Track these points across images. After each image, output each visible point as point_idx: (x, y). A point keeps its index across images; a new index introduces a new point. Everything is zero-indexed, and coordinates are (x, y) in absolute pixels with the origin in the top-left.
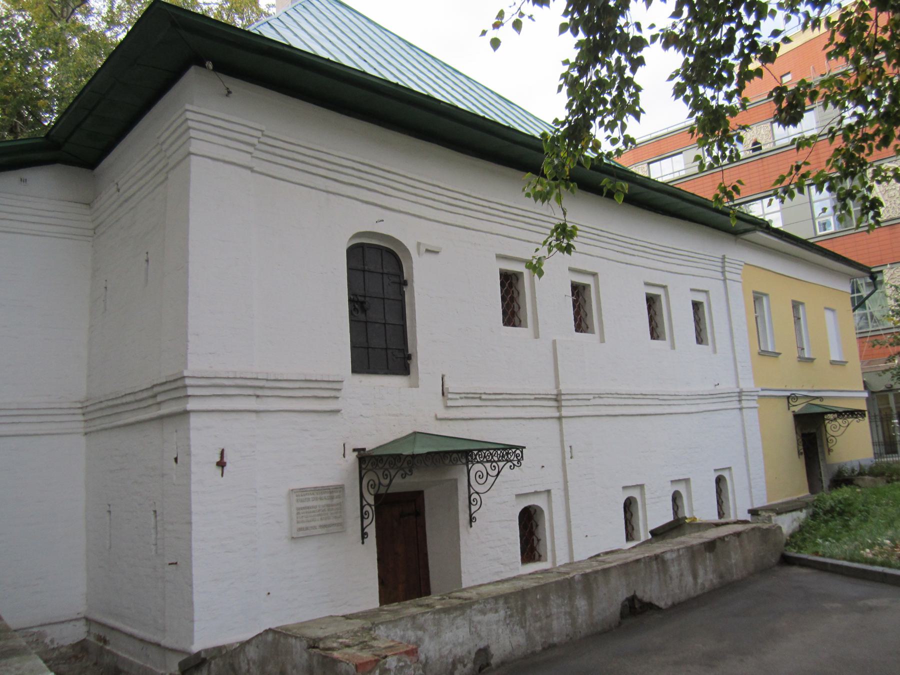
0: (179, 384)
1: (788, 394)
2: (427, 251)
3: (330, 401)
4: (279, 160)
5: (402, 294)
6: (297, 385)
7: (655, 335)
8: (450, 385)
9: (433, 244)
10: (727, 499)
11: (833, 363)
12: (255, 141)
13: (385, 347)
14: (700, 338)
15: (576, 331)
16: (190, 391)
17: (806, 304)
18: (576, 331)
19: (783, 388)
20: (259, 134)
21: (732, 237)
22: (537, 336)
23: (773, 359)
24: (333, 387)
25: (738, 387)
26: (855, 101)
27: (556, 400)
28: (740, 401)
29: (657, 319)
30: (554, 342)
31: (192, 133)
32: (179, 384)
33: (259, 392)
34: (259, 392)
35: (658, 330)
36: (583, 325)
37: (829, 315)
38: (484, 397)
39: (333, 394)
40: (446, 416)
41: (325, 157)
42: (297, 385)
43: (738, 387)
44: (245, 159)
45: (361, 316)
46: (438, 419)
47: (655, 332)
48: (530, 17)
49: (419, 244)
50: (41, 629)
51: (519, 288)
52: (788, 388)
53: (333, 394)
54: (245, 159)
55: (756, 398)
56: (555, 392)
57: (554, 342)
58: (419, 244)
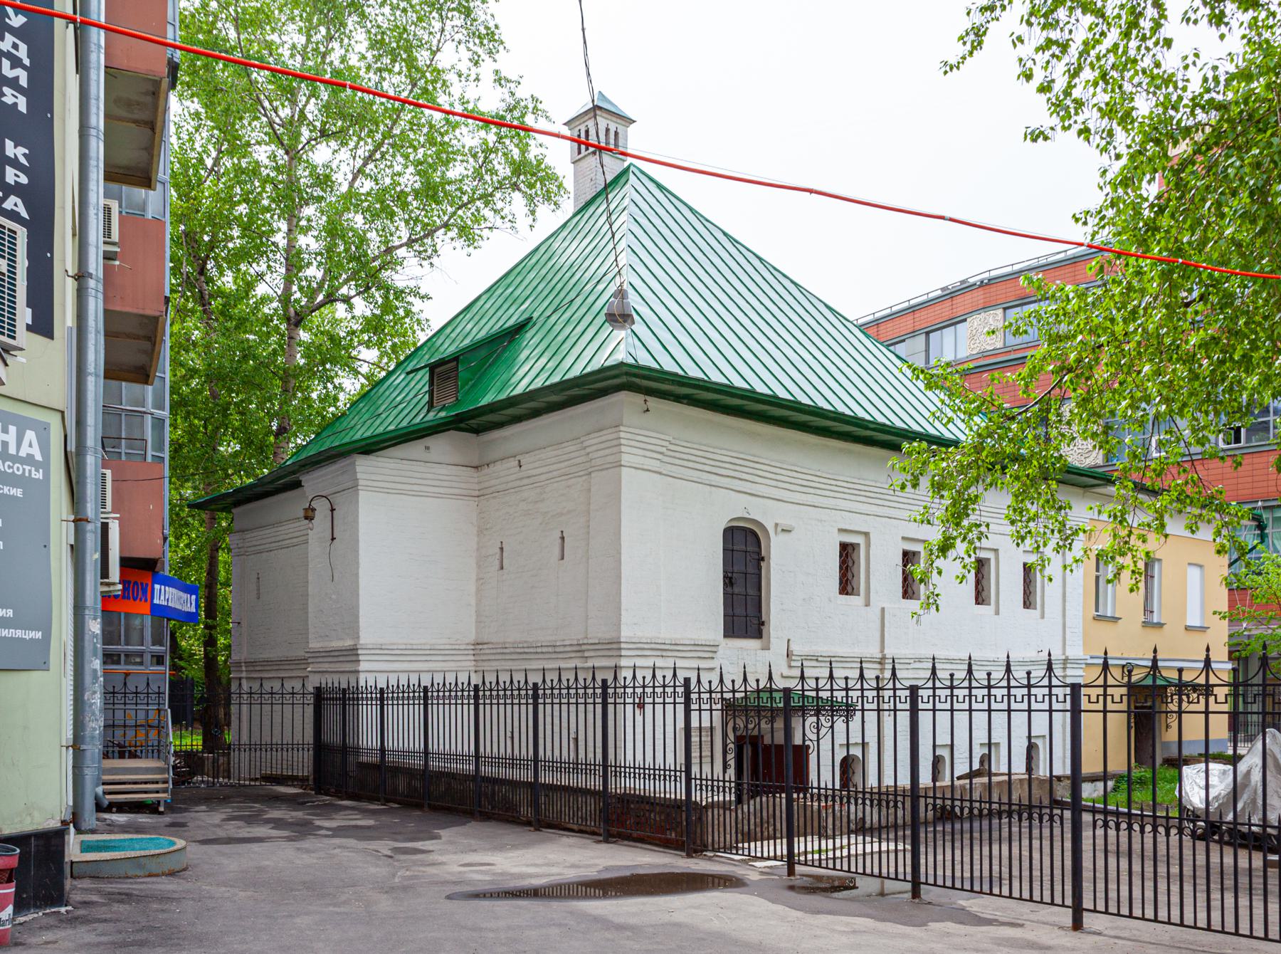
0: (614, 646)
1: (1124, 662)
2: (783, 530)
3: (709, 661)
4: (677, 462)
5: (760, 569)
6: (689, 648)
7: (980, 600)
8: (793, 647)
9: (785, 522)
10: (1038, 767)
11: (1187, 628)
12: (664, 450)
13: (1101, 714)
14: (1028, 603)
15: (840, 593)
16: (623, 653)
17: (1164, 563)
18: (840, 593)
19: (1119, 656)
20: (666, 444)
21: (1080, 491)
22: (867, 604)
23: (1111, 624)
24: (713, 649)
25: (1064, 654)
26: (197, 725)
27: (880, 663)
28: (1064, 668)
29: (984, 582)
30: (883, 610)
31: (623, 449)
32: (614, 646)
33: (664, 654)
34: (664, 654)
35: (984, 594)
36: (849, 588)
37: (1194, 573)
38: (820, 659)
39: (710, 655)
40: (790, 674)
41: (711, 456)
42: (689, 648)
43: (1064, 654)
44: (655, 465)
45: (729, 589)
46: (783, 677)
47: (847, 585)
48: (1037, 136)
49: (777, 525)
50: (636, 317)
51: (855, 557)
52: (1125, 656)
53: (710, 655)
54: (655, 465)
55: (1084, 666)
56: (880, 656)
57: (883, 610)
58: (777, 525)
